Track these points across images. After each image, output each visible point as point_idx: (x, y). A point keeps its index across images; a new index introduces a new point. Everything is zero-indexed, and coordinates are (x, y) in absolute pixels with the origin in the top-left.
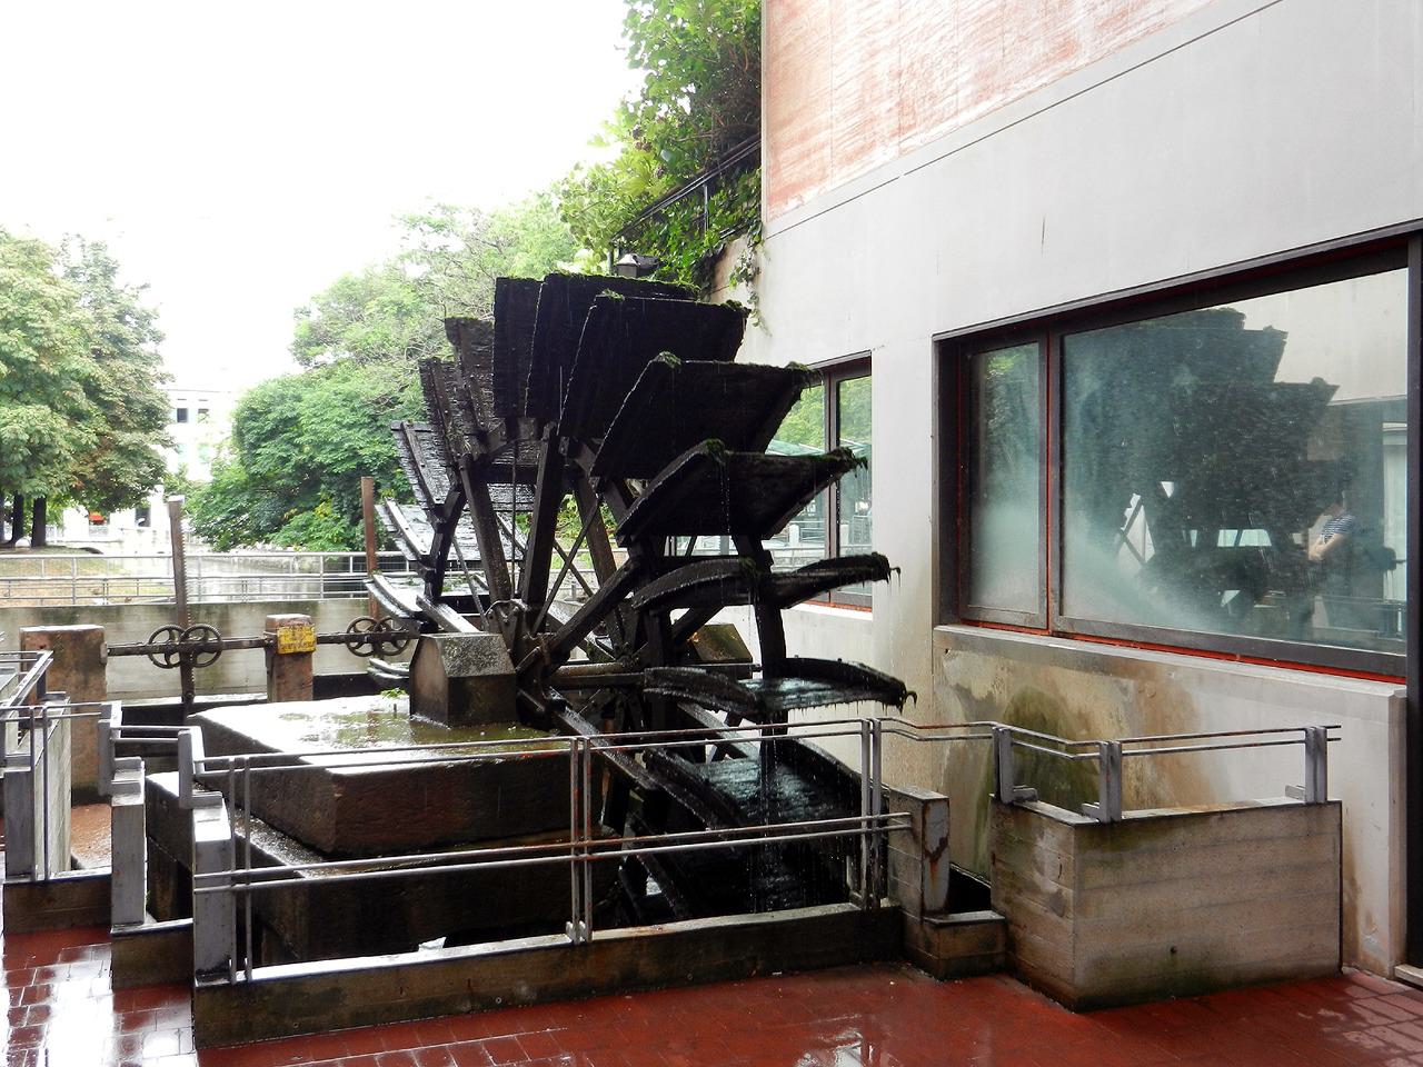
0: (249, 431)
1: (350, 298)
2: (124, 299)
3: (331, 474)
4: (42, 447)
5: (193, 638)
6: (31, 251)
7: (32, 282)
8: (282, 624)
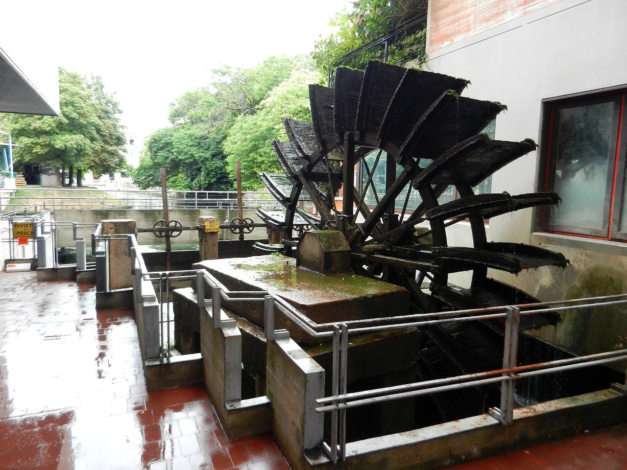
0: (154, 147)
1: (190, 100)
2: (108, 97)
3: (185, 163)
4: (82, 150)
6: (74, 77)
7: (75, 89)
8: (206, 220)
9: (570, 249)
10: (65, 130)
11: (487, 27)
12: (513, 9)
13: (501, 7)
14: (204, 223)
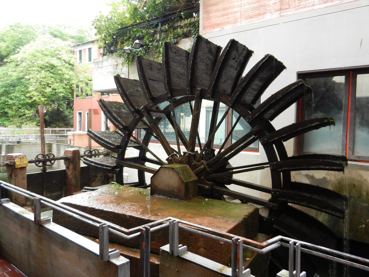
8: (16, 157)
12: (271, 12)
13: (262, 10)
14: (14, 160)
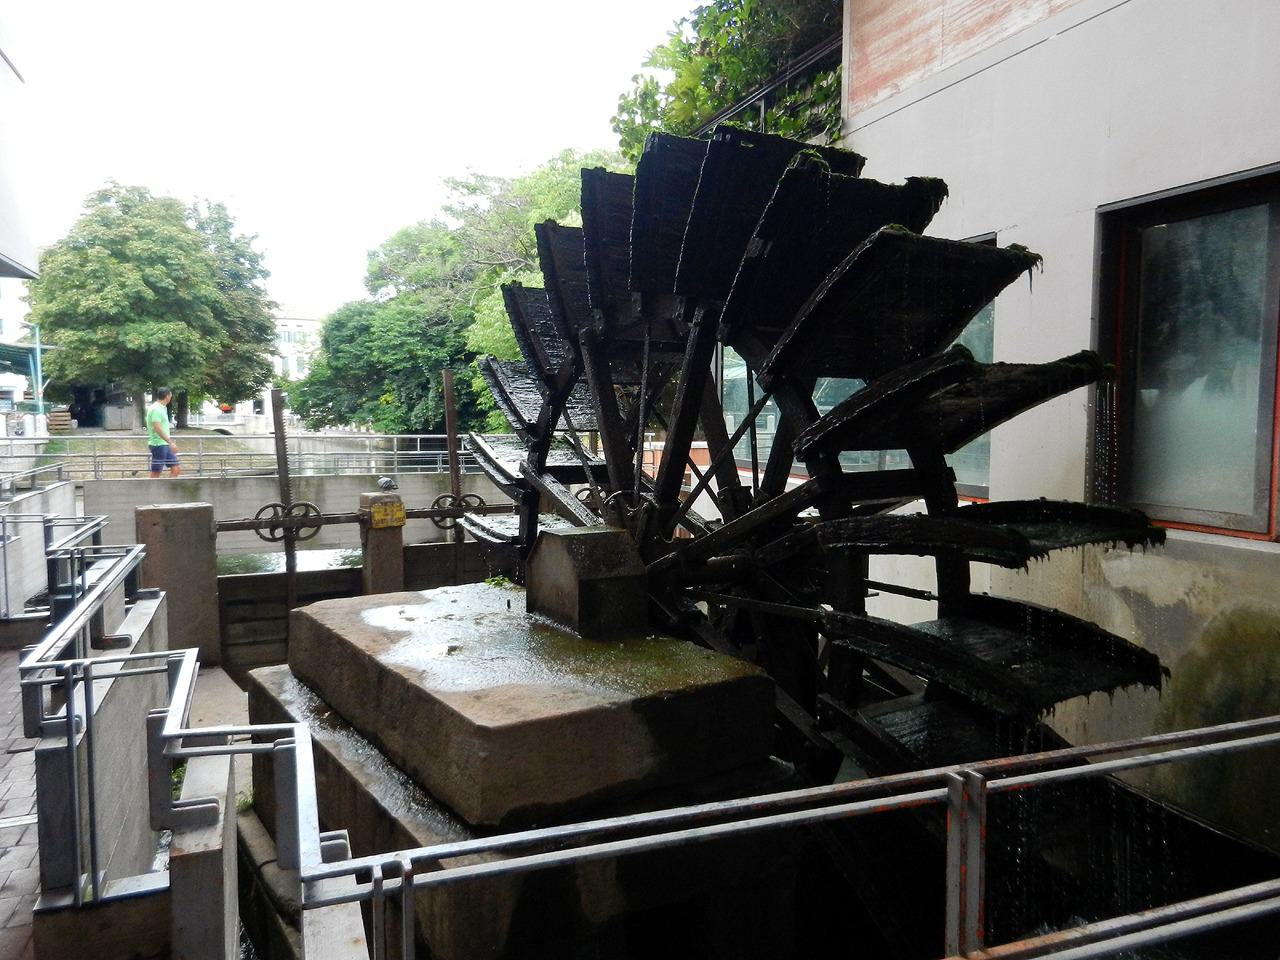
5: (295, 512)
9: (1179, 562)
10: (149, 314)
11: (970, 49)
